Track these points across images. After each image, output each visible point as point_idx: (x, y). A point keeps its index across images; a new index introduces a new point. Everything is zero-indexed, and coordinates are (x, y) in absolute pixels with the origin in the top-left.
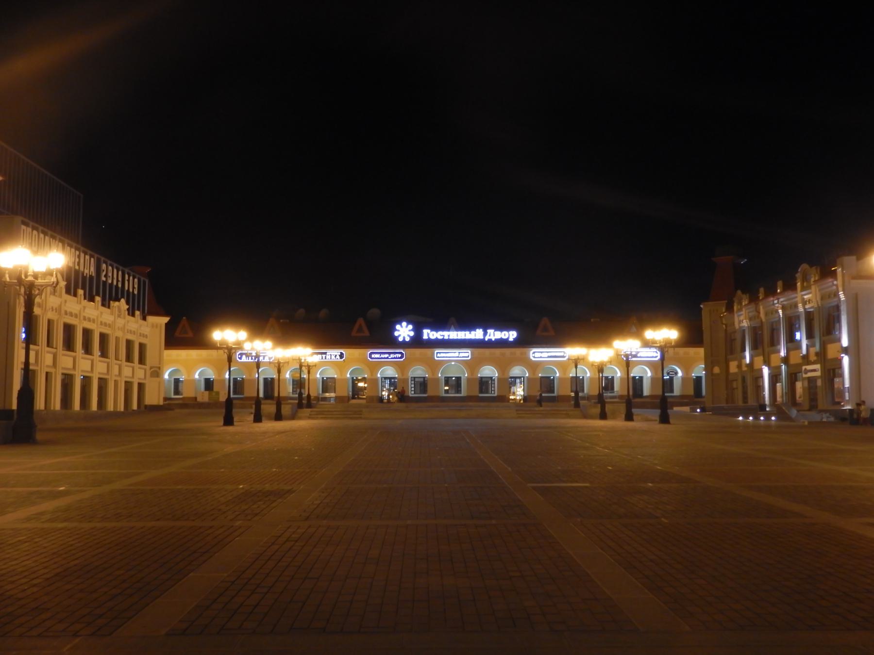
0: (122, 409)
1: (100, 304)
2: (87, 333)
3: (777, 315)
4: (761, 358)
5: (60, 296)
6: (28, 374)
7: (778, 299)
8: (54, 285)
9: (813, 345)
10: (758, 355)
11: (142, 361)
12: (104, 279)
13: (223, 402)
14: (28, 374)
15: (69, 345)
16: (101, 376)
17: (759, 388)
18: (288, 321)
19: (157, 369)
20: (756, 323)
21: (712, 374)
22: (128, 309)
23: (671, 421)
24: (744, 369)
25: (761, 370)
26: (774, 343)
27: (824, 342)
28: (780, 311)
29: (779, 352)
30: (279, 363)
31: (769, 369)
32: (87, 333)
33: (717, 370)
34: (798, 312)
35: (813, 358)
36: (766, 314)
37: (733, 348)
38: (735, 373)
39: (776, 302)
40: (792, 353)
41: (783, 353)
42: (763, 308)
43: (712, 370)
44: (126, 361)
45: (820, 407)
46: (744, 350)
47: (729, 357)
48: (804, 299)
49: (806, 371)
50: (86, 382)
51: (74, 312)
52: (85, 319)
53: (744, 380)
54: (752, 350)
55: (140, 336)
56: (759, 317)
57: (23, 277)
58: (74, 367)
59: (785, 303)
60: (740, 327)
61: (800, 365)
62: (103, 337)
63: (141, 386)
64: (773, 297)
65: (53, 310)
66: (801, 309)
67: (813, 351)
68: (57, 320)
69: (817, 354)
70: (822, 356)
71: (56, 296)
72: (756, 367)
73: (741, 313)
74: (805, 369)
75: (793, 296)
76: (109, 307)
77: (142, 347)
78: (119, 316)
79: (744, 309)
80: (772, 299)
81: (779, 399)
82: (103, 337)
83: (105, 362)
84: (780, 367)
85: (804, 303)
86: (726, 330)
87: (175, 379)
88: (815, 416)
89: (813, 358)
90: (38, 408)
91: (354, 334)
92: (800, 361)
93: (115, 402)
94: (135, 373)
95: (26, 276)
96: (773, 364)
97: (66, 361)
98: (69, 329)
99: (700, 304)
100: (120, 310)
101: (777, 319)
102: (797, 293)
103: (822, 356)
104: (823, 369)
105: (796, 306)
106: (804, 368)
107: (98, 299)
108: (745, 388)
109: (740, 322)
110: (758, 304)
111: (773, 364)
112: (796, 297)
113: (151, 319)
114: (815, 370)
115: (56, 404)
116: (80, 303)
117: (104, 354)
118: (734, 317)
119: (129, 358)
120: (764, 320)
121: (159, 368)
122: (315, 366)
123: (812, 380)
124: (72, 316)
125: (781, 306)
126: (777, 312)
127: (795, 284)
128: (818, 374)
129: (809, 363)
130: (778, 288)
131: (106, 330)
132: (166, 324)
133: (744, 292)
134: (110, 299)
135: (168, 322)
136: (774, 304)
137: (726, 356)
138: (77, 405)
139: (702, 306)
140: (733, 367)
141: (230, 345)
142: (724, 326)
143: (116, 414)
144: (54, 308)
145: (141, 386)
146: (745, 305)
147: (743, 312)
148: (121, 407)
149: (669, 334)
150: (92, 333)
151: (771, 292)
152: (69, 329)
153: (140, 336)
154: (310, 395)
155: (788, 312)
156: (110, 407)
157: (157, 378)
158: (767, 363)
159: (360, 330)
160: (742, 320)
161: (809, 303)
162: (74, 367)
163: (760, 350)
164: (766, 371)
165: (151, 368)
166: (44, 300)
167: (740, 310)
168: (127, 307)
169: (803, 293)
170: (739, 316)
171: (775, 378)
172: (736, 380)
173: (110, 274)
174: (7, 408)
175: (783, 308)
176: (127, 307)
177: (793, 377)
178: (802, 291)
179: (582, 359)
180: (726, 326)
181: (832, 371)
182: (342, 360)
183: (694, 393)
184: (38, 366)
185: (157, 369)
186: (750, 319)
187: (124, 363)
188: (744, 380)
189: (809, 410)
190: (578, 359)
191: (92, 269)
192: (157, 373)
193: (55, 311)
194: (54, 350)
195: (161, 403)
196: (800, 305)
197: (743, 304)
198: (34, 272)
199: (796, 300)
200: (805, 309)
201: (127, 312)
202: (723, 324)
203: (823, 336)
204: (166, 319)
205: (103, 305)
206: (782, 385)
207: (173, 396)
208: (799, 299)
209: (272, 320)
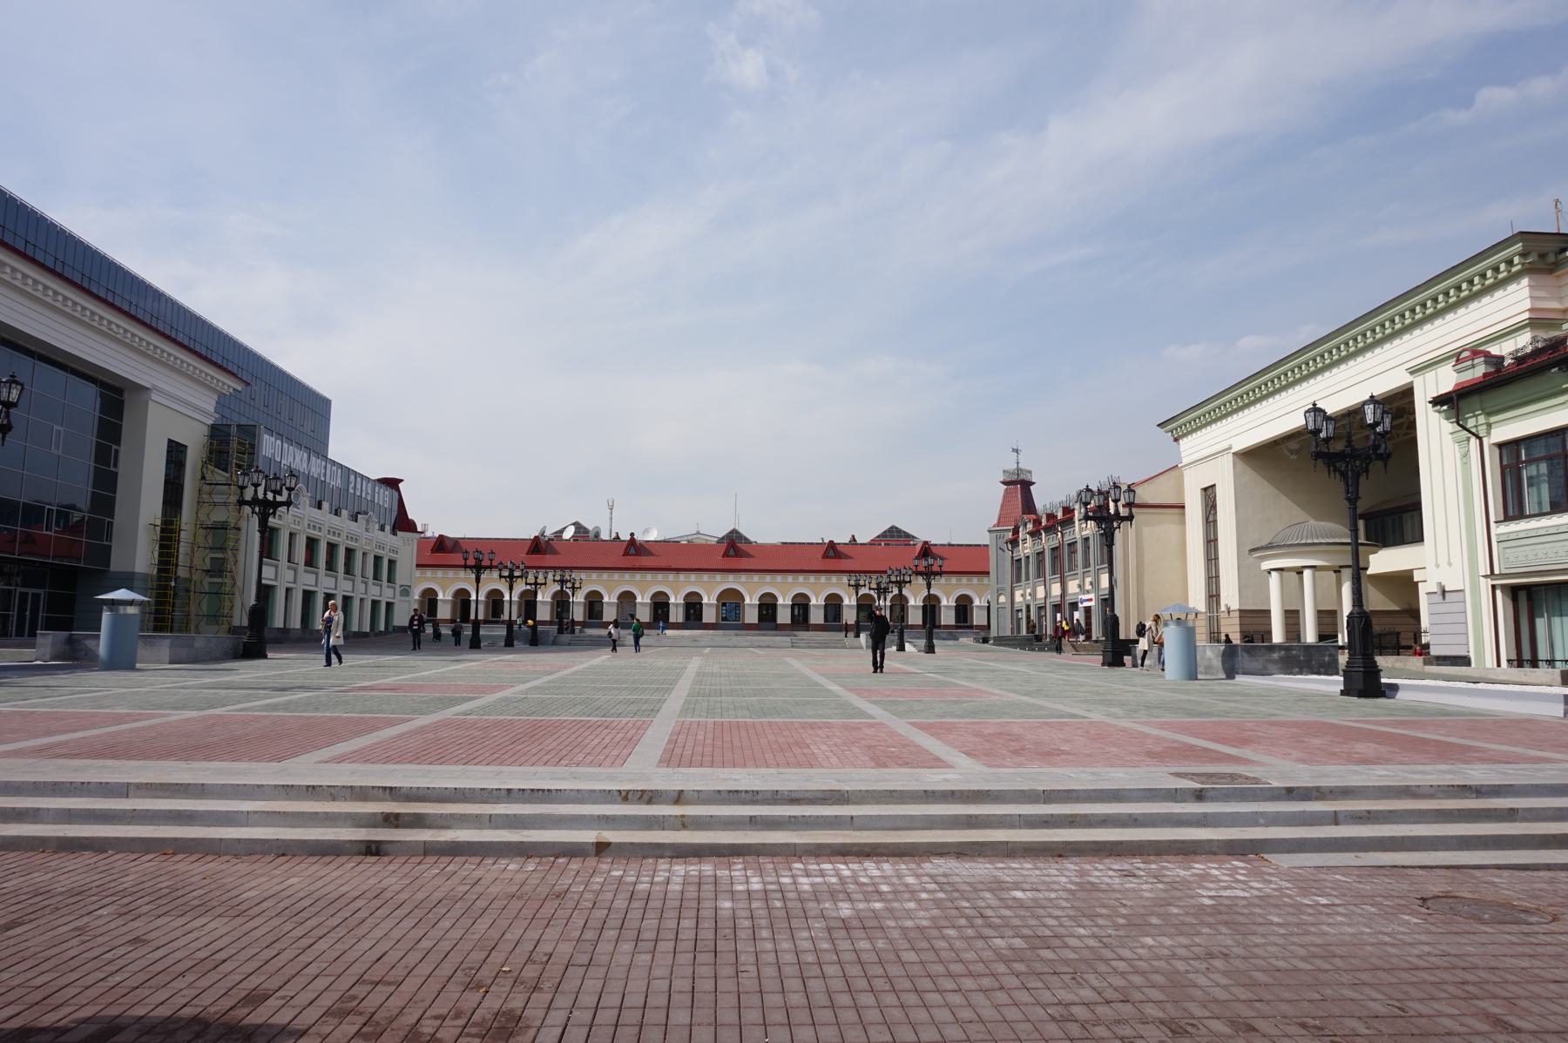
0: (368, 630)
6: (265, 592)
11: (391, 579)
12: (352, 491)
14: (265, 592)
16: (346, 594)
23: (936, 650)
32: (332, 547)
38: (1021, 602)
42: (149, 602)
53: (1028, 607)
62: (350, 552)
63: (389, 605)
83: (313, 573)
104: (1098, 596)
117: (349, 570)
123: (1088, 610)
148: (367, 629)
154: (88, 668)
166: (1120, 873)
173: (359, 486)
182: (586, 589)
183: (249, 622)
188: (1028, 607)
191: (339, 480)
192: (406, 591)
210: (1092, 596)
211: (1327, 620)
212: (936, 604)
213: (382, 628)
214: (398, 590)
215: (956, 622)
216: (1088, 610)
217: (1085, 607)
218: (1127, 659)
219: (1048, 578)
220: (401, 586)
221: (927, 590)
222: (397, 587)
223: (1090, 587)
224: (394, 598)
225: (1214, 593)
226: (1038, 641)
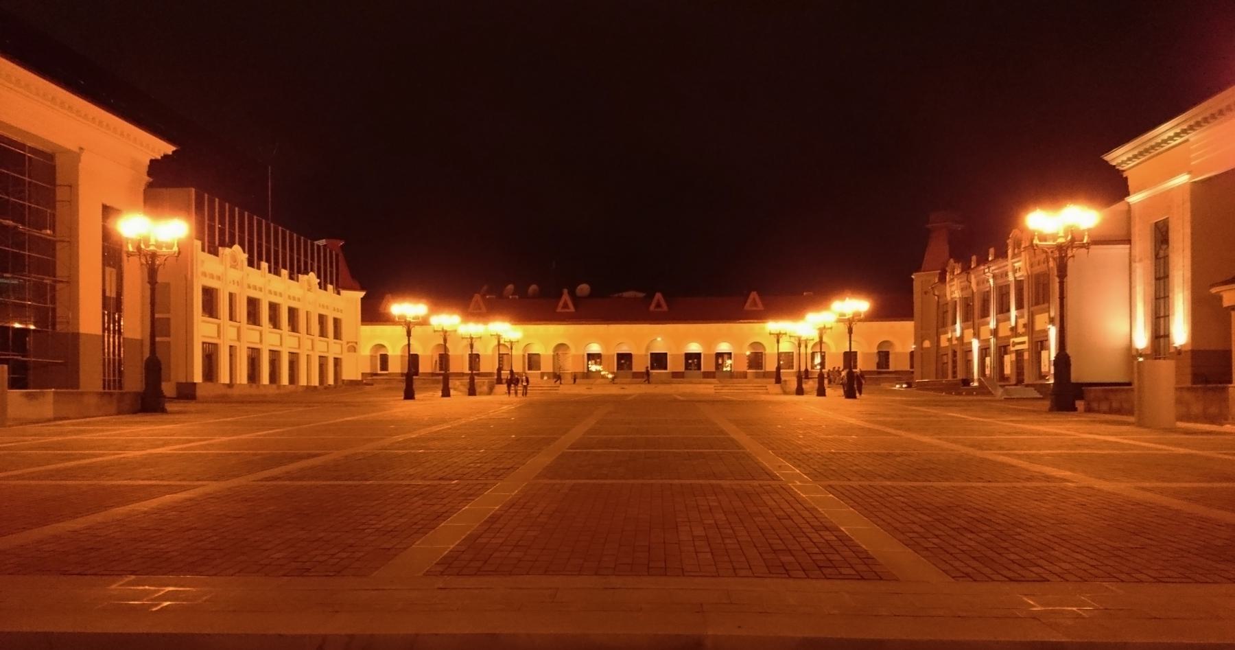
1: (287, 277)
2: (274, 308)
3: (988, 285)
4: (971, 331)
5: (242, 270)
7: (989, 268)
8: (176, 255)
9: (1022, 316)
10: (968, 328)
11: (337, 335)
13: (78, 330)
15: (253, 317)
17: (968, 362)
18: (494, 296)
19: (355, 345)
20: (967, 294)
21: (922, 349)
22: (319, 284)
24: (955, 342)
25: (971, 343)
26: (985, 313)
27: (1032, 312)
28: (991, 281)
29: (988, 324)
30: (445, 332)
31: (979, 342)
32: (274, 308)
33: (927, 344)
34: (1009, 281)
35: (1021, 330)
36: (978, 284)
37: (944, 322)
39: (987, 270)
40: (1001, 325)
41: (992, 325)
42: (975, 277)
43: (922, 343)
44: (320, 336)
45: (1026, 382)
46: (954, 323)
47: (940, 330)
48: (1014, 266)
49: (1015, 344)
50: (275, 357)
51: (278, 291)
52: (270, 292)
53: (955, 353)
54: (963, 322)
55: (334, 310)
56: (970, 287)
57: (143, 246)
58: (261, 341)
59: (996, 271)
60: (952, 298)
61: (1008, 338)
62: (292, 312)
63: (337, 362)
64: (984, 265)
65: (234, 284)
66: (1011, 278)
67: (1022, 321)
68: (240, 293)
69: (1025, 326)
70: (1030, 326)
71: (237, 269)
72: (966, 341)
73: (953, 283)
74: (1013, 342)
75: (1005, 264)
76: (298, 281)
77: (337, 322)
78: (309, 290)
79: (956, 280)
80: (982, 267)
81: (988, 372)
82: (292, 312)
84: (988, 340)
85: (1015, 271)
86: (938, 302)
87: (381, 355)
88: (1020, 391)
89: (1021, 330)
90: (238, 382)
91: (559, 310)
92: (1009, 333)
93: (308, 376)
94: (332, 348)
95: (147, 245)
96: (982, 337)
97: (251, 336)
98: (253, 304)
99: (912, 274)
100: (309, 284)
101: (988, 289)
102: (1007, 261)
103: (1030, 326)
104: (1031, 341)
105: (1007, 275)
106: (1012, 340)
107: (285, 272)
108: (954, 362)
109: (952, 292)
110: (969, 273)
111: (982, 337)
112: (1007, 265)
113: (344, 293)
114: (1022, 342)
115: (242, 377)
116: (265, 277)
117: (294, 327)
118: (945, 289)
119: (323, 333)
120: (975, 291)
121: (356, 343)
122: (518, 342)
123: (1019, 354)
124: (256, 289)
125: (992, 275)
126: (988, 281)
127: (1006, 252)
128: (1025, 346)
129: (1017, 335)
130: (990, 255)
131: (294, 304)
132: (362, 299)
133: (957, 261)
134: (299, 272)
135: (364, 296)
136: (984, 273)
137: (937, 330)
138: (285, 379)
139: (913, 277)
140: (944, 343)
141: (408, 319)
142: (936, 297)
143: (309, 389)
144: (236, 282)
145: (337, 362)
146: (958, 274)
147: (956, 282)
148: (315, 382)
149: (856, 305)
150: (259, 304)
151: (983, 260)
152: (253, 304)
153: (334, 310)
155: (1000, 281)
156: (303, 381)
157: (354, 354)
158: (977, 335)
159: (566, 306)
160: (954, 291)
161: (1020, 271)
162: (261, 341)
163: (970, 323)
164: (976, 345)
165: (348, 343)
167: (952, 280)
168: (319, 280)
169: (1013, 260)
170: (951, 286)
171: (984, 352)
172: (947, 354)
174: (189, 381)
175: (994, 277)
176: (319, 280)
177: (1003, 350)
178: (1012, 258)
179: (784, 334)
180: (938, 298)
181: (1039, 343)
184: (220, 338)
185: (355, 345)
186: (962, 289)
187: (317, 338)
188: (955, 353)
189: (1016, 385)
190: (780, 333)
192: (353, 348)
193: (236, 284)
194: (238, 324)
195: (360, 378)
196: (1010, 274)
197: (956, 273)
198: (156, 241)
199: (1006, 268)
200: (1015, 278)
201: (318, 286)
202: (935, 295)
203: (1032, 306)
204: (362, 294)
205: (291, 278)
206: (991, 359)
207: (379, 372)
208: (1009, 268)
209: (477, 297)
210: (1025, 339)
211: (590, 357)
212: (763, 351)
213: (331, 381)
214: (345, 347)
215: (878, 367)
216: (1019, 354)
217: (1017, 351)
218: (1080, 404)
219: (977, 321)
220: (348, 343)
221: (470, 350)
222: (344, 342)
223: (1023, 330)
224: (342, 353)
225: (1162, 333)
226: (964, 385)
